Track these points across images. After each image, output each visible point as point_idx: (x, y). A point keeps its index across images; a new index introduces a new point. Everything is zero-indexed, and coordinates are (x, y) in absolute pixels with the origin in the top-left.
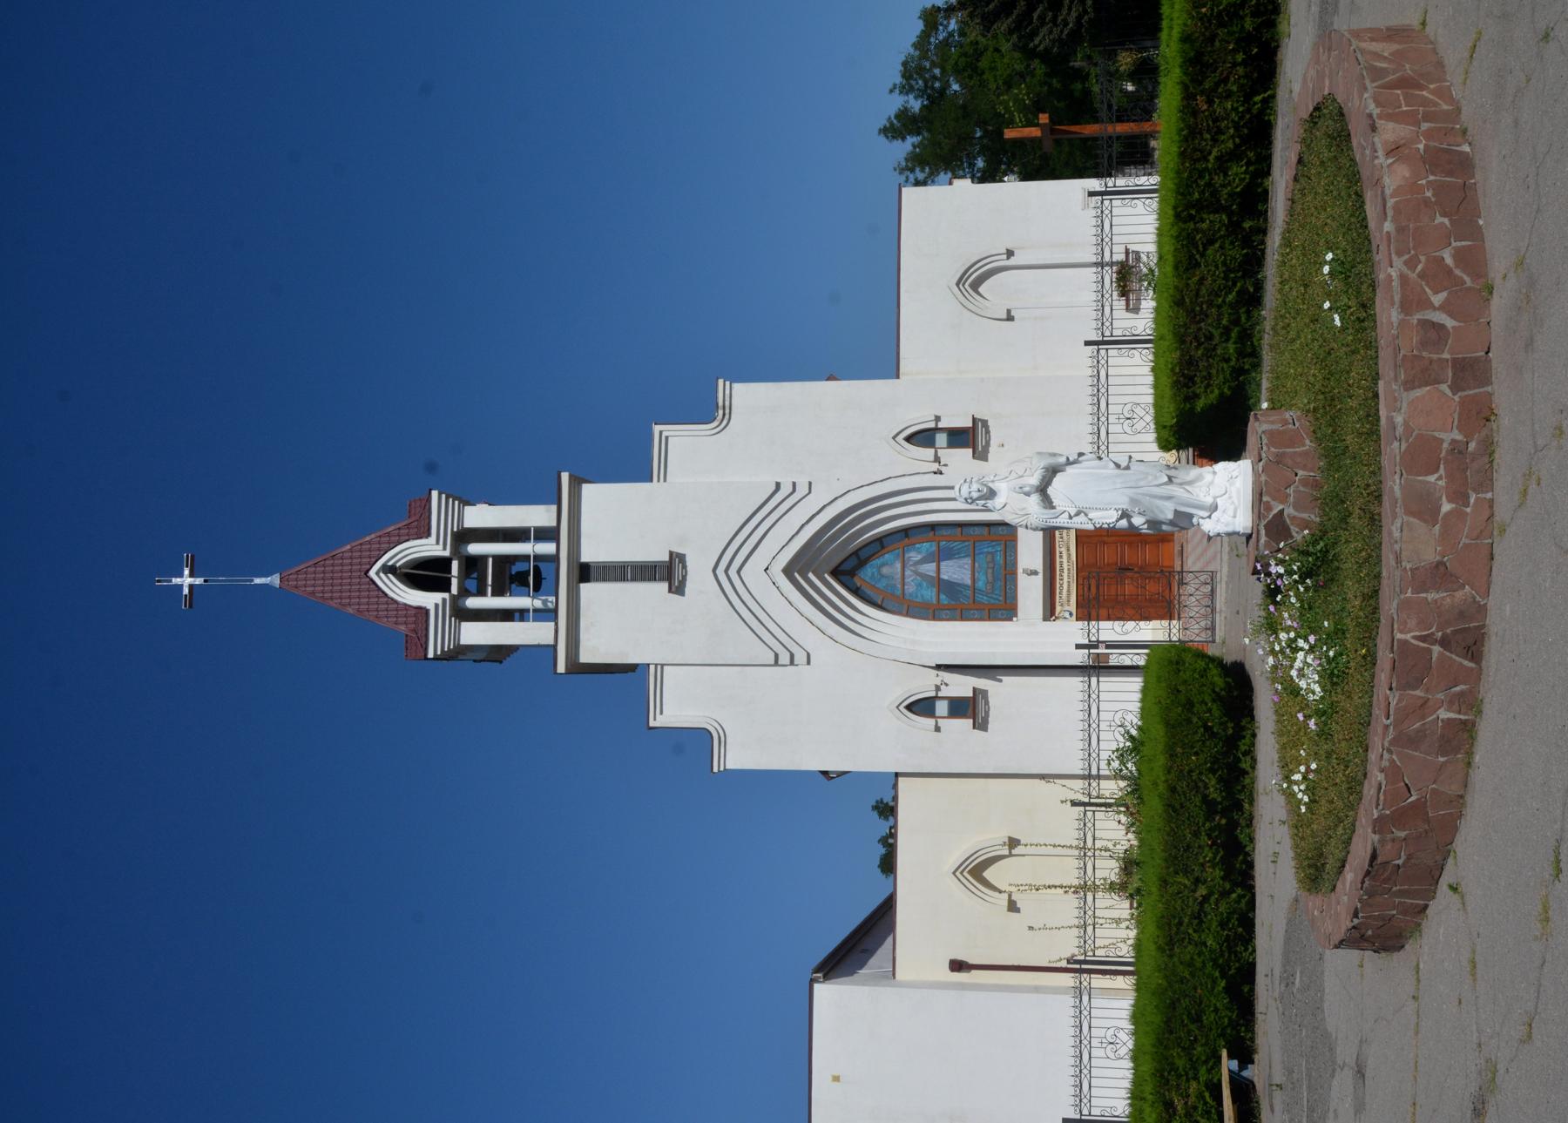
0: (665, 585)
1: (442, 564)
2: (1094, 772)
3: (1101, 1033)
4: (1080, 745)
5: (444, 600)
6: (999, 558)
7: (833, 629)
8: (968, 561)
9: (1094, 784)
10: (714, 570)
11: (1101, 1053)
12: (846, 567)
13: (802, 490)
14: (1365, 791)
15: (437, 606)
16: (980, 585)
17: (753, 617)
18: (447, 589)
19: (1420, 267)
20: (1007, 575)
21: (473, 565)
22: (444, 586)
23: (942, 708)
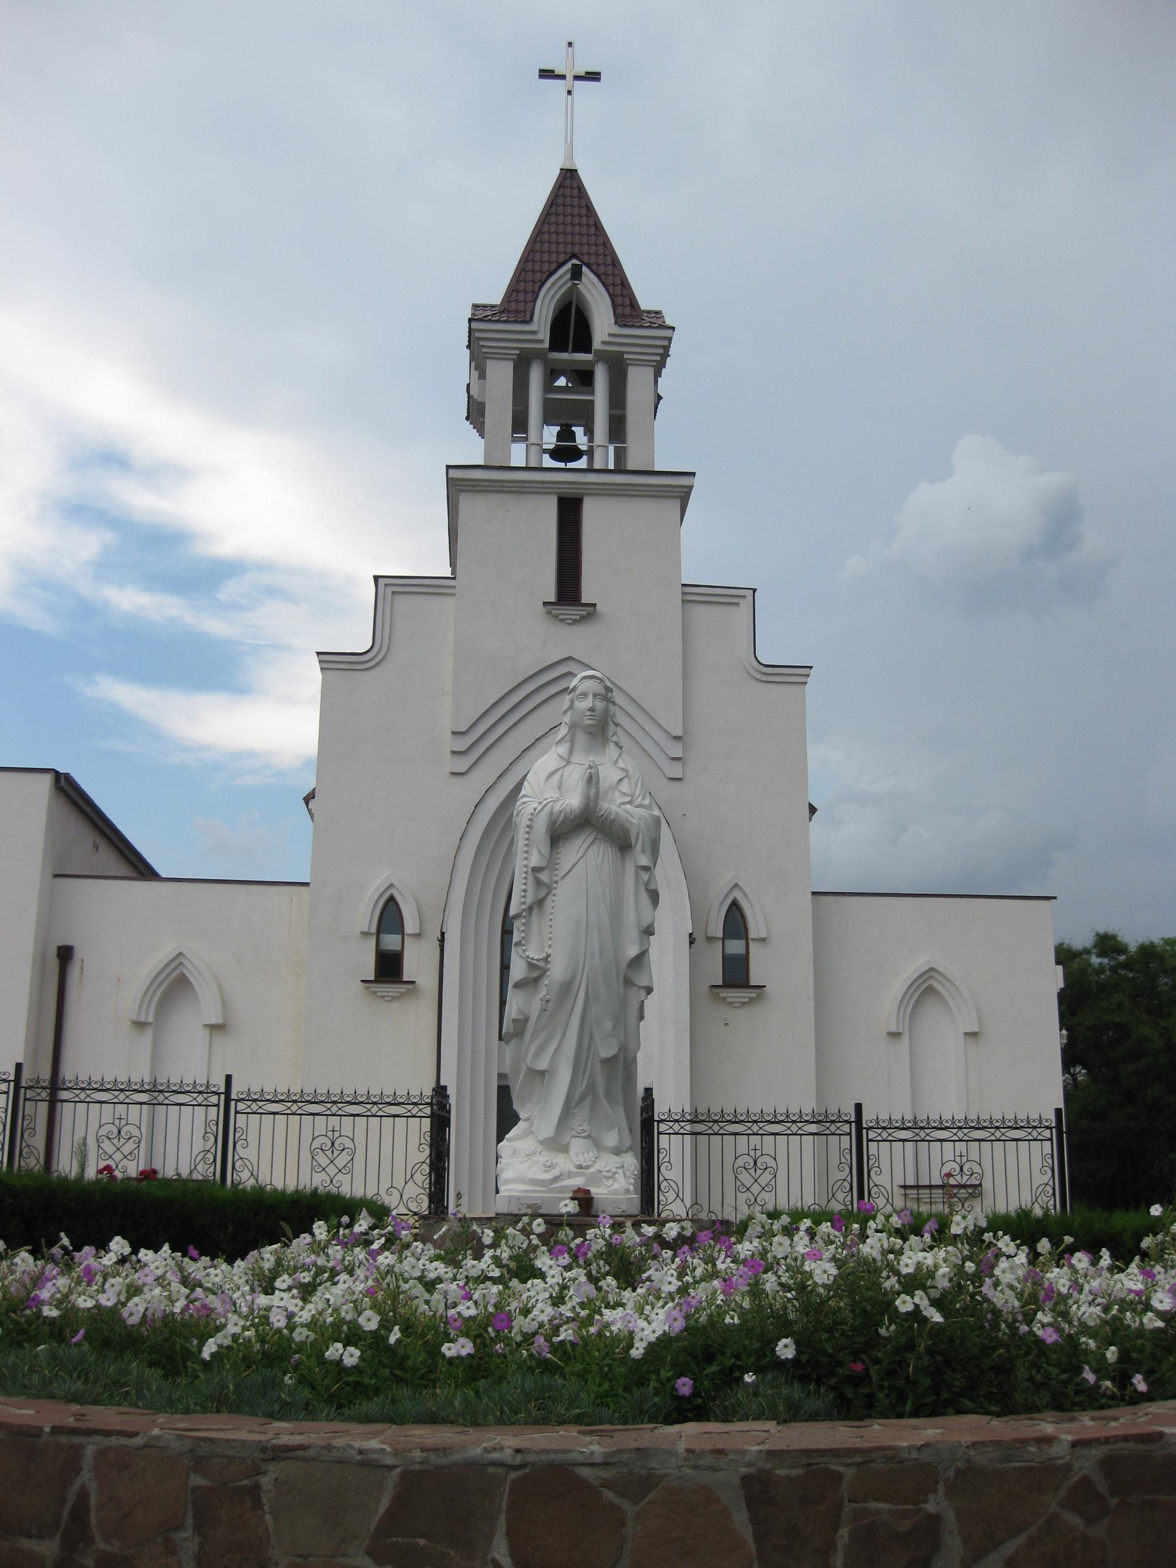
0: (552, 597)
1: (584, 342)
2: (64, 1095)
3: (974, 1155)
4: (388, 1091)
5: (541, 341)
9: (44, 1094)
10: (570, 658)
11: (948, 1155)
13: (676, 771)
14: (967, 1438)
15: (534, 333)
19: (1075, 1520)
21: (584, 378)
22: (558, 343)
23: (735, 947)
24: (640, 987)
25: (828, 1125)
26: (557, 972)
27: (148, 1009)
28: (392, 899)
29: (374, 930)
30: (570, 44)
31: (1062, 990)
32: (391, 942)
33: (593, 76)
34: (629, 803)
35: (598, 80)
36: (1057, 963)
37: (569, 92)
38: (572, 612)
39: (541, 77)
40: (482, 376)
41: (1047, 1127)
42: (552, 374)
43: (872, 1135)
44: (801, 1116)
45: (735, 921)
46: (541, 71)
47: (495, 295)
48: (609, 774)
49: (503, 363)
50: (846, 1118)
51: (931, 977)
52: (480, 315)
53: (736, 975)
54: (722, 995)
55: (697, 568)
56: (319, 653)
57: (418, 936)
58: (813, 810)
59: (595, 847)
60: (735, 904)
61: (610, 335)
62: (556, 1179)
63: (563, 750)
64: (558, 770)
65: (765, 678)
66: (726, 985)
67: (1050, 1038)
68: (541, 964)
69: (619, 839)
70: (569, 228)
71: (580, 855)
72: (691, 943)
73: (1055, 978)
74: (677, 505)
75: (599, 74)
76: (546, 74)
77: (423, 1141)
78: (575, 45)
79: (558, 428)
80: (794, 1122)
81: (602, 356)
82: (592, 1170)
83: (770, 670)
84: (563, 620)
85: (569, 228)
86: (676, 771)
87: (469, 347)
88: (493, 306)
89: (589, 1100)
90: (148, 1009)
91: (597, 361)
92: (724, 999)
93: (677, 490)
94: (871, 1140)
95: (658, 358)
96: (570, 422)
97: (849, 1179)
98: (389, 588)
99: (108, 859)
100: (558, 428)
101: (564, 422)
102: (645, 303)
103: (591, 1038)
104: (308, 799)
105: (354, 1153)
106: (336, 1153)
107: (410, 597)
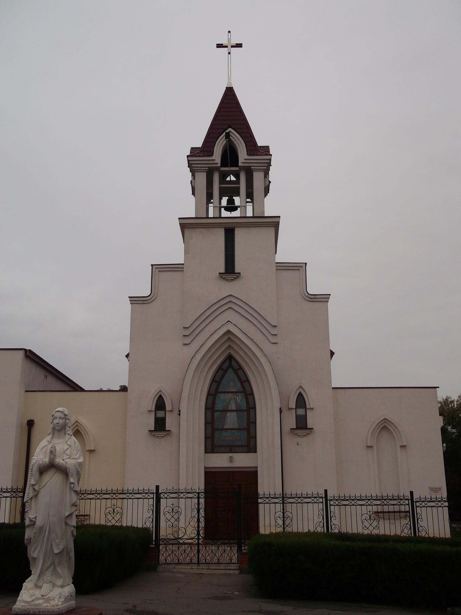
0: (223, 271)
5: (217, 164)
6: (238, 443)
7: (199, 357)
8: (237, 427)
10: (231, 295)
12: (234, 363)
13: (273, 340)
15: (214, 160)
16: (224, 433)
17: (206, 317)
18: (222, 165)
20: (231, 448)
23: (301, 412)
24: (71, 526)
25: (313, 499)
26: (39, 523)
27: (205, 366)
28: (161, 396)
29: (153, 409)
30: (229, 32)
31: (442, 427)
32: (160, 414)
33: (239, 45)
34: (69, 458)
35: (241, 47)
36: (440, 415)
37: (229, 53)
38: (230, 277)
39: (217, 47)
40: (194, 179)
41: (407, 499)
42: (223, 176)
43: (332, 503)
44: (302, 495)
45: (301, 401)
46: (217, 45)
47: (199, 144)
48: (59, 448)
49: (202, 173)
50: (321, 496)
51: (385, 422)
52: (194, 152)
53: (302, 425)
54: (296, 432)
55: (282, 256)
56: (129, 297)
57: (171, 411)
58: (332, 354)
59: (55, 475)
60: (300, 394)
61: (245, 159)
62: (33, 601)
63: (51, 436)
64: (45, 446)
65: (311, 300)
66: (298, 428)
67: (438, 448)
68: (34, 520)
69: (64, 471)
70: (230, 114)
71: (49, 479)
72: (281, 412)
73: (440, 421)
74: (272, 230)
75: (242, 44)
76: (219, 46)
77: (150, 508)
78: (231, 32)
79: (227, 198)
80: (299, 498)
81: (243, 168)
82: (47, 597)
83: (312, 297)
84: (227, 280)
85: (230, 114)
86: (273, 340)
87: (188, 167)
88: (199, 148)
89: (52, 568)
90: (205, 366)
91: (241, 170)
92: (297, 434)
93: (274, 224)
94: (331, 505)
95: (265, 168)
96: (232, 195)
97: (322, 522)
98: (158, 269)
99: (53, 383)
100: (227, 198)
101: (230, 195)
102: (260, 142)
103: (52, 546)
104: (127, 356)
105: (122, 514)
106: (115, 514)
107: (166, 273)
